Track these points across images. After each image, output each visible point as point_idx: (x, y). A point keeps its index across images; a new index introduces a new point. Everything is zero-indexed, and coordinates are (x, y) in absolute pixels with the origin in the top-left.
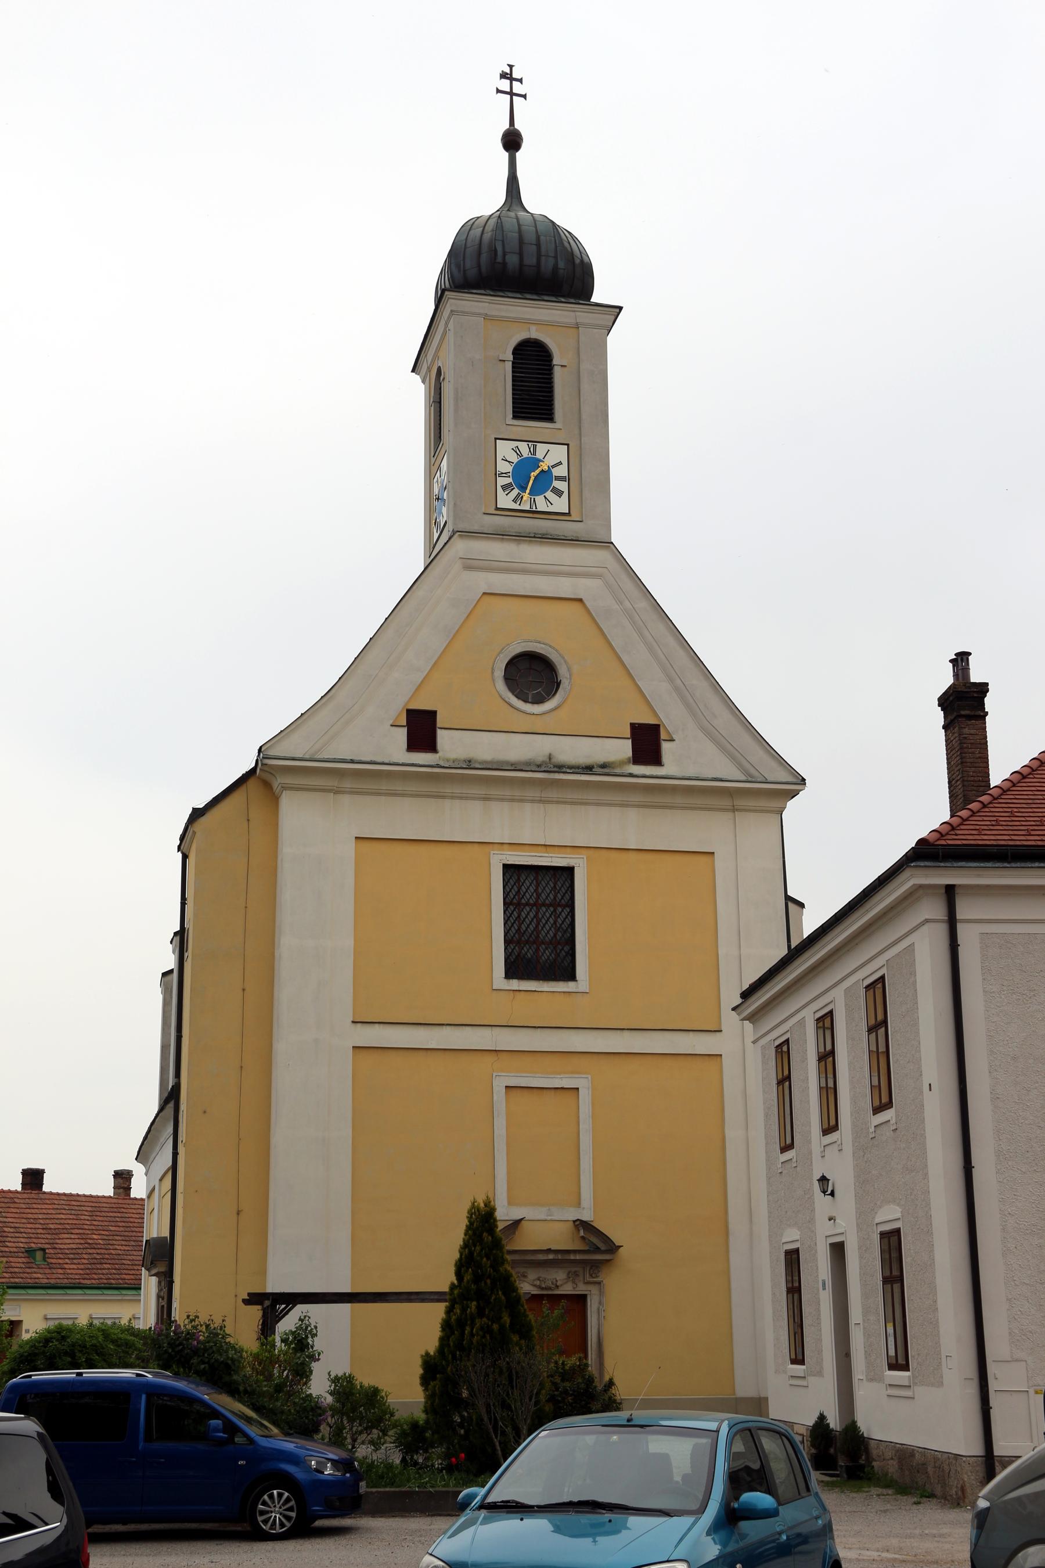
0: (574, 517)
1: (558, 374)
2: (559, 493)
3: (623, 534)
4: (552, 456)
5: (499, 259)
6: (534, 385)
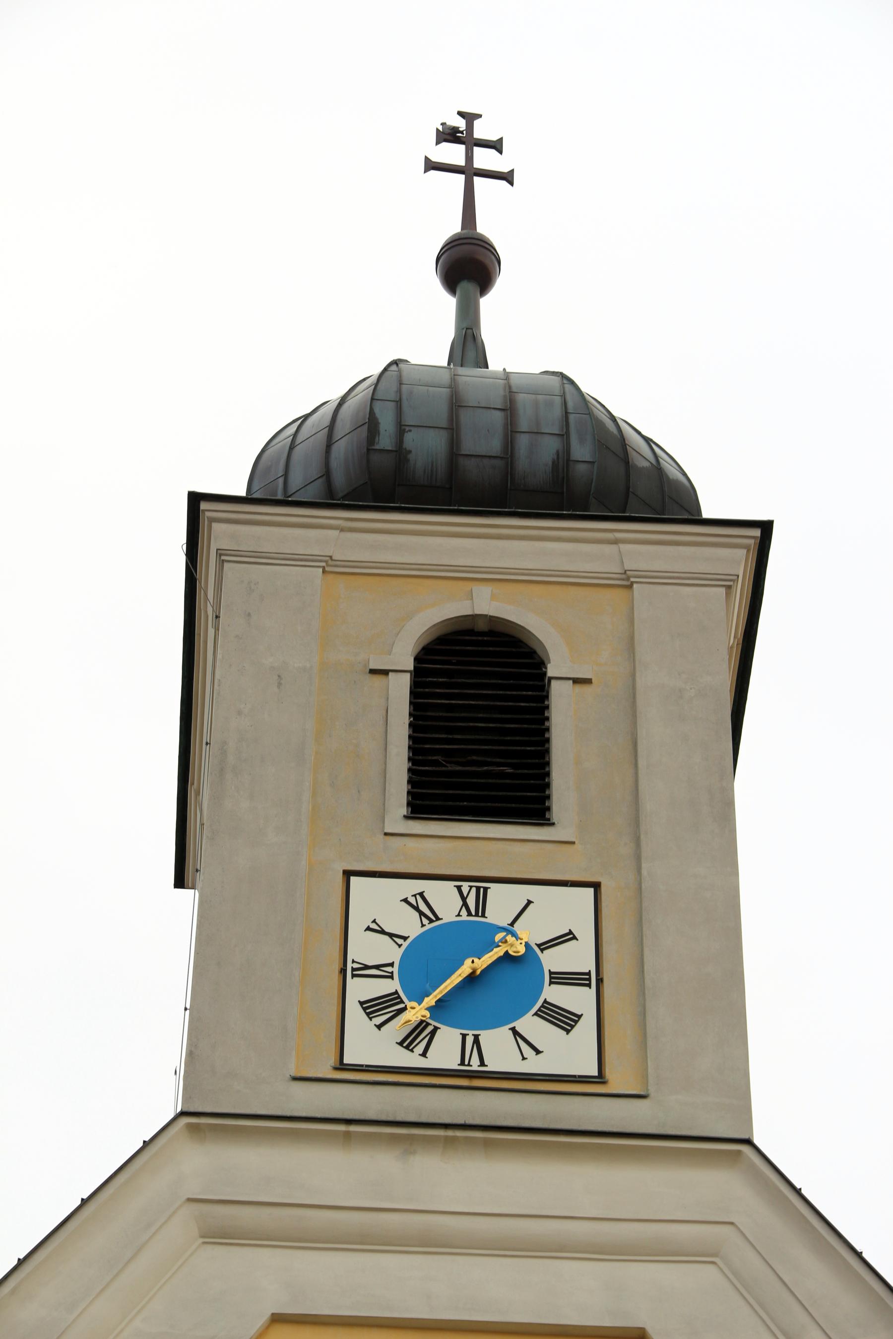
0: (617, 1082)
1: (564, 709)
2: (565, 1020)
3: (792, 1121)
4: (546, 917)
5: (385, 441)
6: (480, 731)
